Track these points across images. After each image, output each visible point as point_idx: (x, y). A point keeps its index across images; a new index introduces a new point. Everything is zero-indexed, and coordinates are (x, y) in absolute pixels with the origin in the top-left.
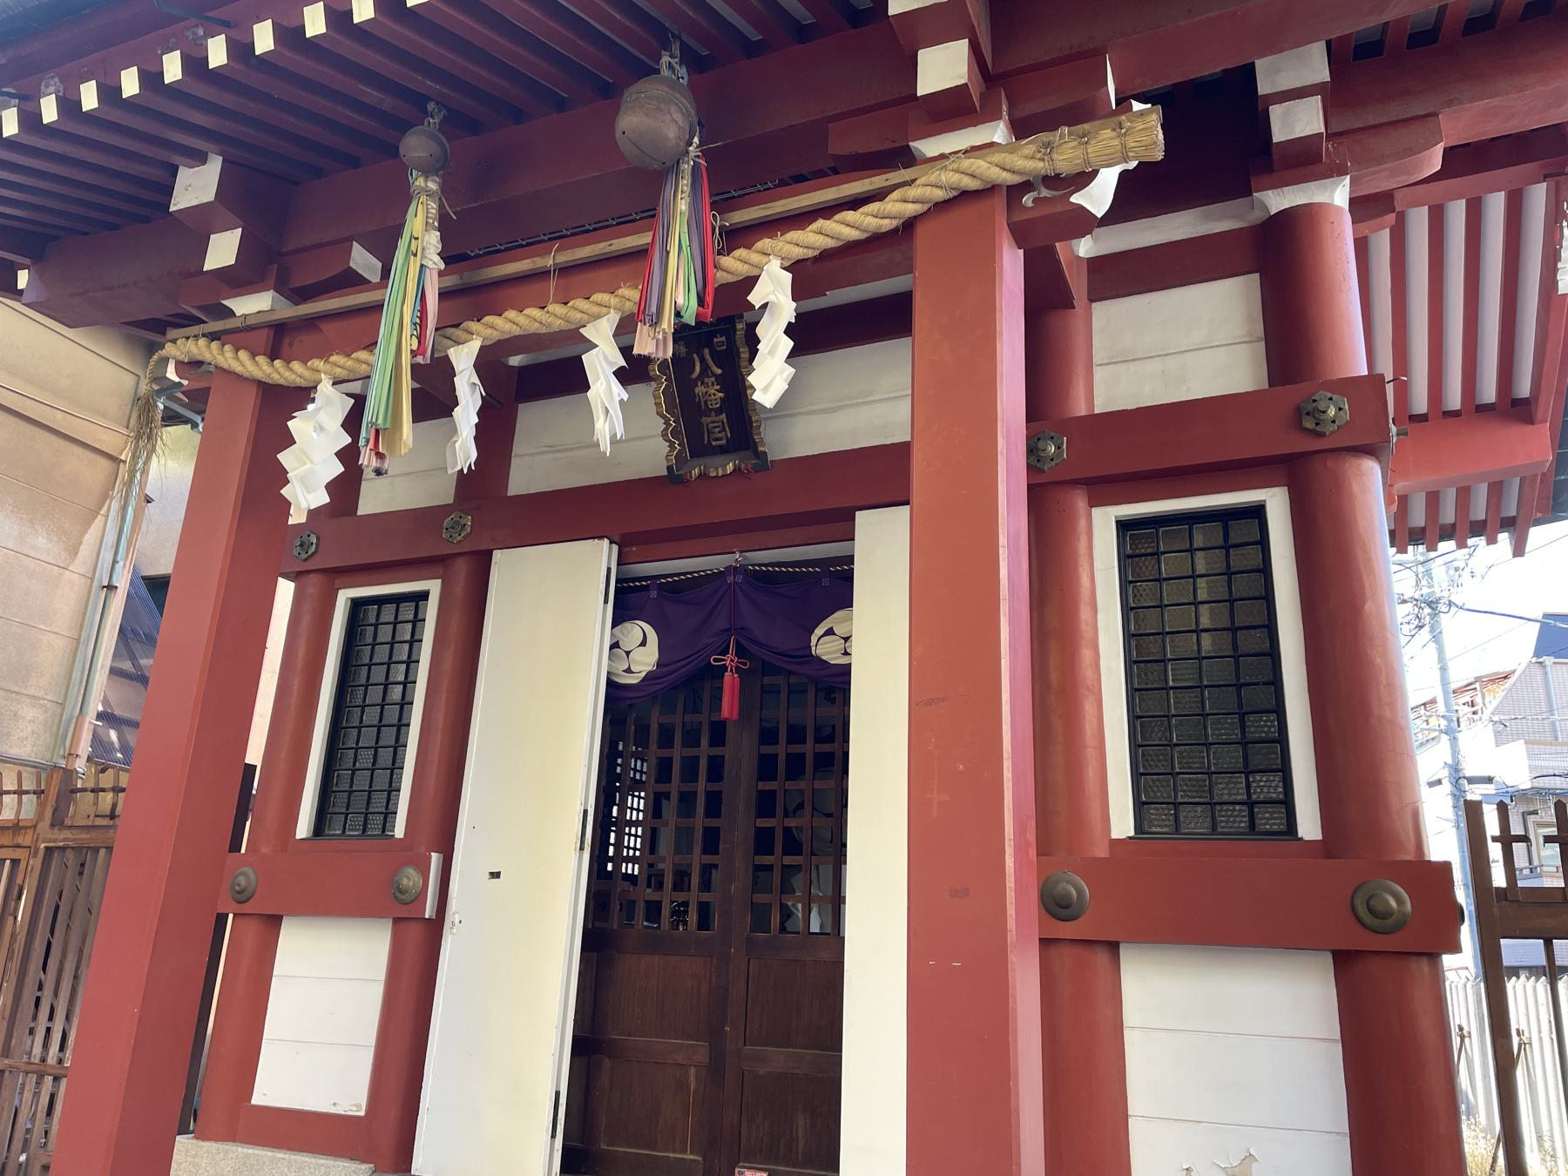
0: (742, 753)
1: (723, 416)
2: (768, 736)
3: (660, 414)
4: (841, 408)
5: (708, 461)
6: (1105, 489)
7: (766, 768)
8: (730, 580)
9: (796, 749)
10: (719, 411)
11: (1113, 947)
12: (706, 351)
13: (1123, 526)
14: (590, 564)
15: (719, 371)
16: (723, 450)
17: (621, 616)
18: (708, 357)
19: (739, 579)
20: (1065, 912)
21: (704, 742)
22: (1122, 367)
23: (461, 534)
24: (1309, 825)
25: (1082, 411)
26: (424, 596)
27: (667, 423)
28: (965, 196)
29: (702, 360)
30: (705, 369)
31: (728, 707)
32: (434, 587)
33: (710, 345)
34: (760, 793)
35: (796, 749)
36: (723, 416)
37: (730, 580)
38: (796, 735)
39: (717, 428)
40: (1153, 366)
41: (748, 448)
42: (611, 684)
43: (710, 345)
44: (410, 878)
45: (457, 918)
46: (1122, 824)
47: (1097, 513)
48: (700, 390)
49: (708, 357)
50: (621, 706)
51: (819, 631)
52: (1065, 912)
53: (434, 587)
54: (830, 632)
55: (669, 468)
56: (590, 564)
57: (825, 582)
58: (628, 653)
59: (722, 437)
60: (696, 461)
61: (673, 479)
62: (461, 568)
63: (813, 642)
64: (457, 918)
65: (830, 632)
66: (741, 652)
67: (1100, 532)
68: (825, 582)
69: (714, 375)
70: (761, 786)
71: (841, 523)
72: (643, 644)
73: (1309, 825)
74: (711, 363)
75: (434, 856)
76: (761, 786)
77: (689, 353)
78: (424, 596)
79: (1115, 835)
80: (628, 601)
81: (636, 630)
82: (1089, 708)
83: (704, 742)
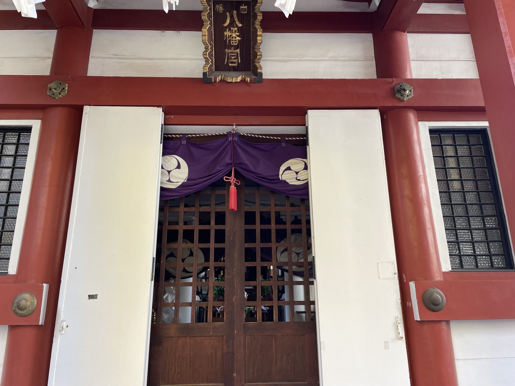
0: (235, 228)
1: (238, 51)
2: (250, 218)
3: (204, 43)
4: (289, 61)
5: (226, 73)
6: (425, 112)
7: (250, 236)
8: (230, 139)
9: (266, 227)
10: (236, 47)
11: (448, 322)
12: (235, 12)
13: (432, 131)
14: (150, 120)
15: (240, 25)
16: (235, 69)
17: (167, 151)
18: (235, 16)
19: (236, 139)
20: (435, 308)
21: (213, 222)
22: (423, 62)
23: (59, 92)
25: (409, 78)
26: (28, 130)
27: (207, 48)
29: (232, 17)
30: (232, 24)
31: (233, 203)
32: (36, 125)
33: (238, 9)
34: (246, 249)
35: (266, 227)
36: (238, 51)
37: (230, 139)
38: (265, 219)
39: (234, 56)
40: (436, 64)
41: (249, 70)
42: (162, 189)
43: (238, 9)
44: (27, 299)
45: (65, 324)
46: (446, 265)
47: (420, 124)
48: (227, 33)
49: (235, 16)
50: (169, 200)
51: (283, 168)
52: (435, 308)
53: (36, 125)
54: (289, 169)
55: (204, 74)
56: (150, 120)
57: (284, 145)
58: (169, 172)
59: (235, 62)
60: (217, 73)
61: (205, 80)
62: (58, 117)
63: (281, 173)
64: (65, 324)
66: (238, 175)
67: (421, 132)
68: (284, 145)
69: (237, 26)
70: (247, 245)
71: (299, 115)
72: (179, 167)
74: (236, 19)
75: (45, 285)
76: (247, 245)
77: (225, 12)
78: (28, 130)
79: (444, 270)
80: (170, 145)
81: (173, 160)
82: (426, 210)
83: (213, 222)
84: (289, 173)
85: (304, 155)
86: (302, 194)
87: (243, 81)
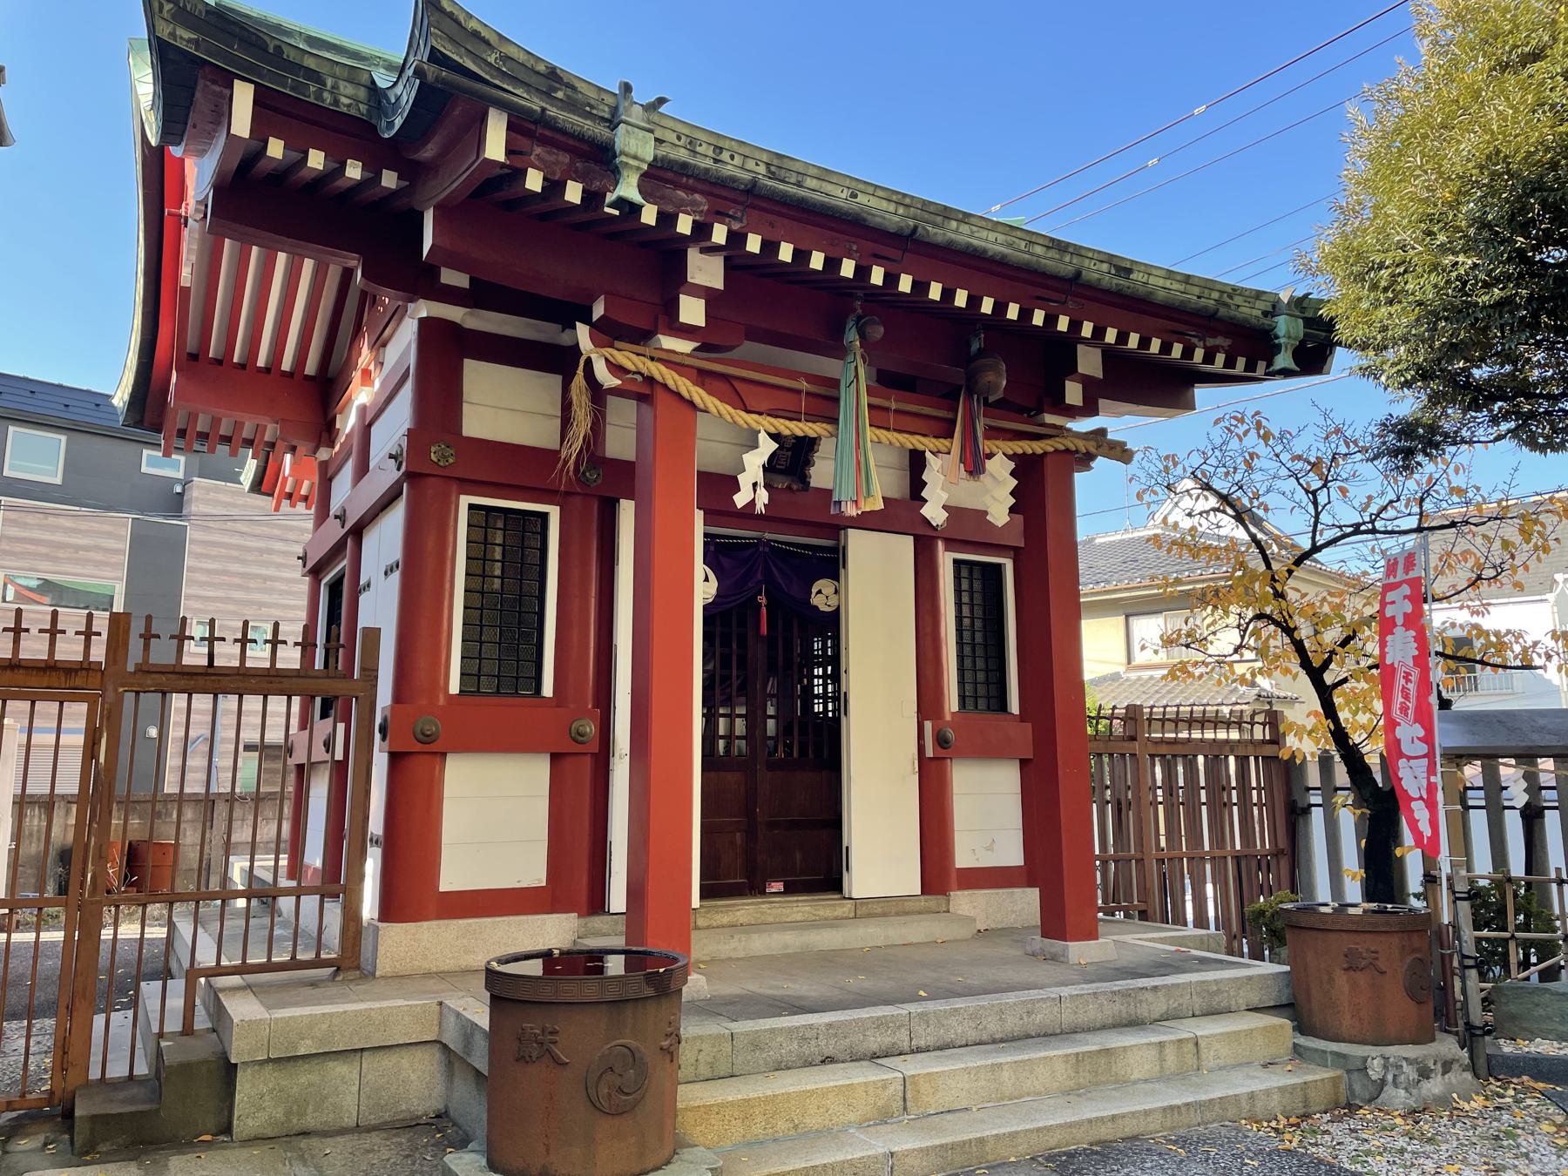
24: (548, 690)
28: (1067, 451)
65: (819, 592)
73: (548, 690)
84: (822, 596)
85: (835, 577)
86: (831, 623)
87: (789, 487)
